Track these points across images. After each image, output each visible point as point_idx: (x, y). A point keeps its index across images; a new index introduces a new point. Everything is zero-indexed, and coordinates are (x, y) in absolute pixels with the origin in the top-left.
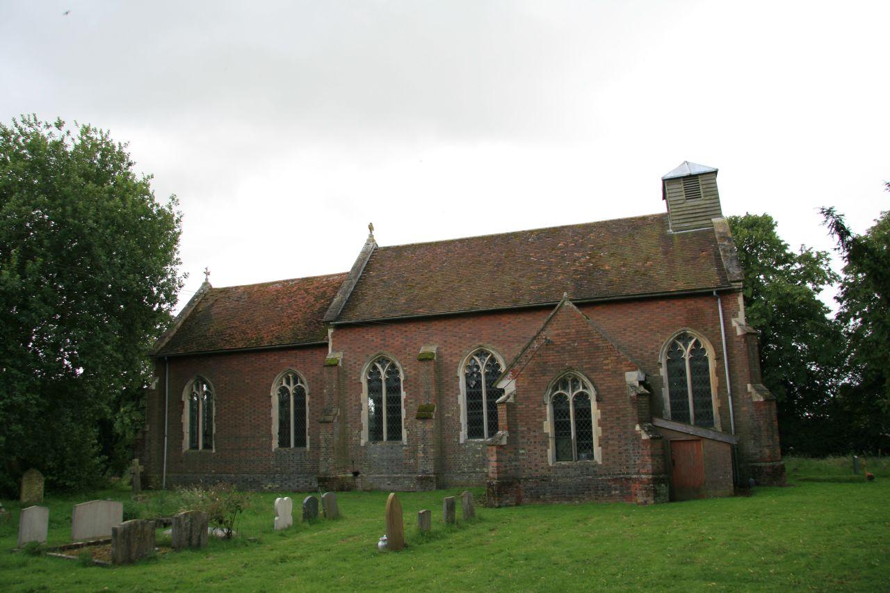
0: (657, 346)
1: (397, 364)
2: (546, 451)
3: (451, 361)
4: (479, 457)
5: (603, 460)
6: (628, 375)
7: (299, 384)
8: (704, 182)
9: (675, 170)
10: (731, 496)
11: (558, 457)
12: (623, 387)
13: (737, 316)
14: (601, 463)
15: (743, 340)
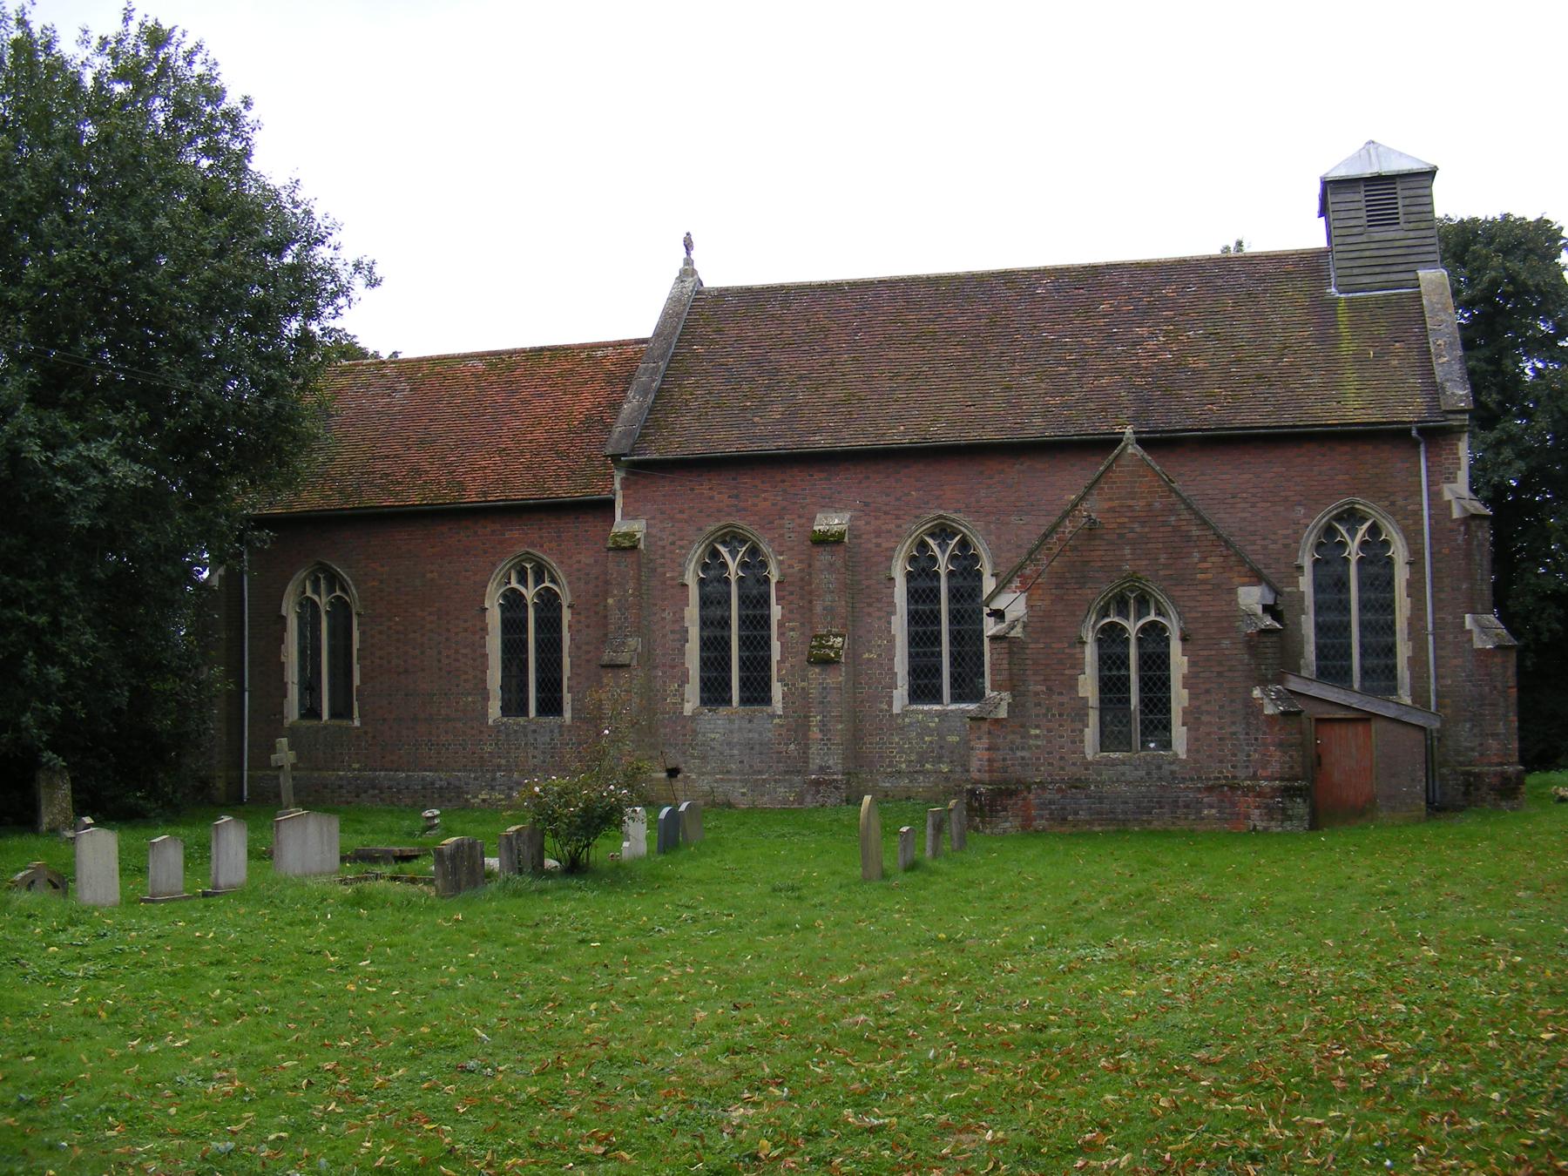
0: (1296, 532)
1: (764, 547)
2: (1082, 731)
3: (878, 545)
4: (931, 742)
5: (1188, 751)
6: (1243, 592)
7: (547, 584)
8: (1407, 193)
9: (1337, 167)
10: (1418, 821)
11: (1105, 743)
12: (1234, 614)
13: (1454, 480)
14: (1184, 757)
15: (1462, 528)
